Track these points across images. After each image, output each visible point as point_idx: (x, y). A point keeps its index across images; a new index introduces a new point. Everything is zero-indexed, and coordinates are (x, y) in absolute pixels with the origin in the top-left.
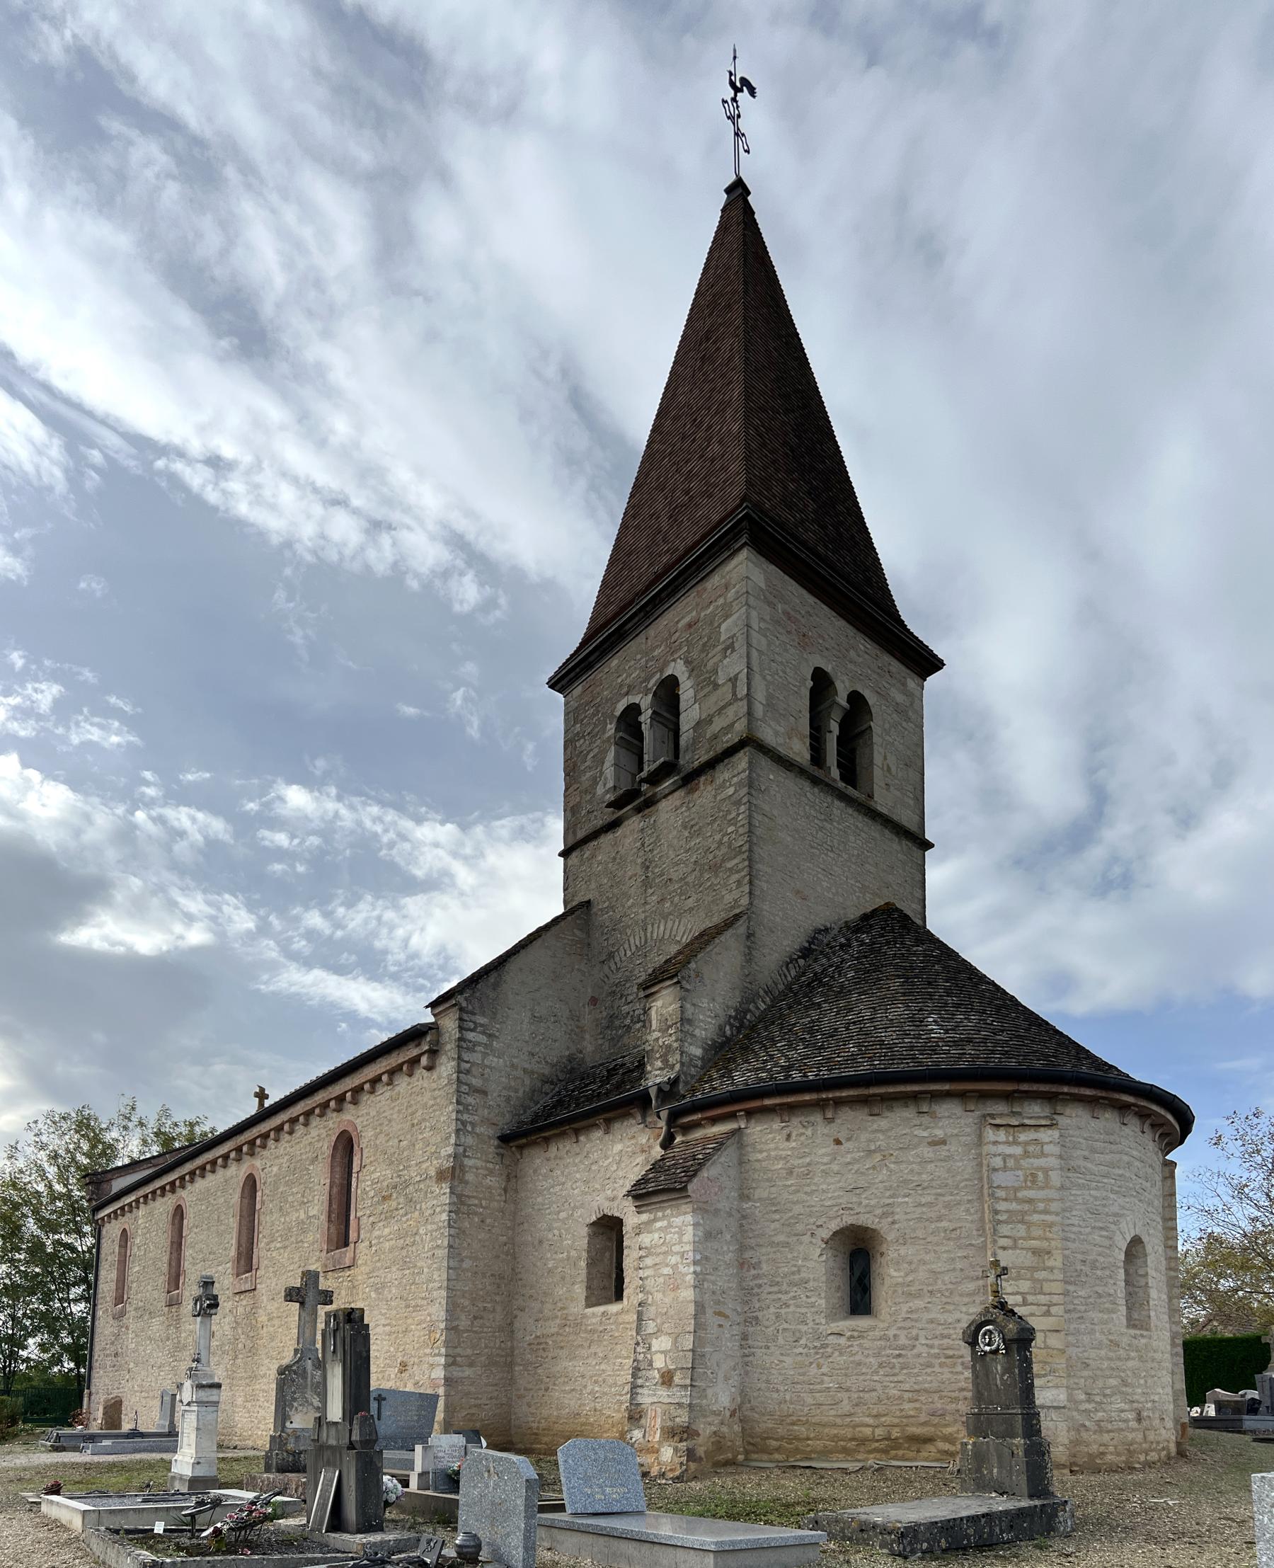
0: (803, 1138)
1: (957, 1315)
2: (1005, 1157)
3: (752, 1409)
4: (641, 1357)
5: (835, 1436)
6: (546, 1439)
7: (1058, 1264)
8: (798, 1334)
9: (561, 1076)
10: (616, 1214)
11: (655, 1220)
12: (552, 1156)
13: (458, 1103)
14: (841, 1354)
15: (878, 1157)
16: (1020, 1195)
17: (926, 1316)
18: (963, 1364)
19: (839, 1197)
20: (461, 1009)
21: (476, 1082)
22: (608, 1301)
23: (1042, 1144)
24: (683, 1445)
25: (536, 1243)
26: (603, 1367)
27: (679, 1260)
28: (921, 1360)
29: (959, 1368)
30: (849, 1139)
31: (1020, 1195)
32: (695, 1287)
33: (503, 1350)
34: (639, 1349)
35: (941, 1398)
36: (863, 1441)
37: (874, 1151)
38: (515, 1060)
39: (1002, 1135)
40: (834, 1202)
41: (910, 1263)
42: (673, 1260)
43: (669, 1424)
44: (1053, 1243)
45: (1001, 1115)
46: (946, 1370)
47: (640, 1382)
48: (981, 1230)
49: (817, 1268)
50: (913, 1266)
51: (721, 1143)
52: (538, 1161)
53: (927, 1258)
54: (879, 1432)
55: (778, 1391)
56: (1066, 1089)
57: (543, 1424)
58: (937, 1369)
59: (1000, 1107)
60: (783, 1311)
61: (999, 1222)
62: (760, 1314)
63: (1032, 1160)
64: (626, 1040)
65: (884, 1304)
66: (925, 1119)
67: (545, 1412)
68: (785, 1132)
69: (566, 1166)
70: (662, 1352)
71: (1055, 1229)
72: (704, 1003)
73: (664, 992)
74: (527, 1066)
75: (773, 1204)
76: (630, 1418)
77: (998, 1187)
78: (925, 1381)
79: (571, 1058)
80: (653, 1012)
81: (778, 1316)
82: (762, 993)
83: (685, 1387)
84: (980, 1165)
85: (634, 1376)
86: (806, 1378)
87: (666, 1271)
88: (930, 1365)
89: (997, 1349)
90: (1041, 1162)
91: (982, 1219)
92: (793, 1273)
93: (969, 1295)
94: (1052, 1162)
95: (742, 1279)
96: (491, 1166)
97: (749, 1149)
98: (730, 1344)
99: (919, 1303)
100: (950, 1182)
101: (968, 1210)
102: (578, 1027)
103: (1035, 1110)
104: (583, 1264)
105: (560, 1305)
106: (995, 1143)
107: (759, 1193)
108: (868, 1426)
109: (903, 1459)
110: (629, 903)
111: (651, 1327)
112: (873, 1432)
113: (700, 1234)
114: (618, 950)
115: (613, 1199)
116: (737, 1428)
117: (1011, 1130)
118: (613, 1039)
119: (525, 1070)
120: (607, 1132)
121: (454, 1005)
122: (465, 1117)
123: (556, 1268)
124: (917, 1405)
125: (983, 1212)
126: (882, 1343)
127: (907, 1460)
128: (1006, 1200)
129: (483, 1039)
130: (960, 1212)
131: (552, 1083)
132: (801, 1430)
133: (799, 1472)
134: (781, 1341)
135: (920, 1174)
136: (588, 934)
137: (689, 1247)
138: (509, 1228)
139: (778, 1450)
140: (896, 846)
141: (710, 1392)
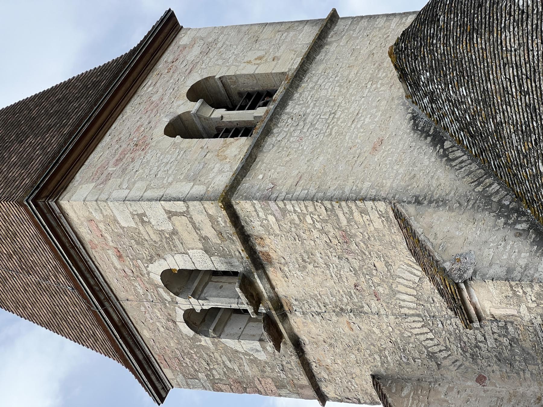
73: (476, 299)
80: (498, 312)
82: (480, 189)
110: (377, 331)
118: (525, 360)
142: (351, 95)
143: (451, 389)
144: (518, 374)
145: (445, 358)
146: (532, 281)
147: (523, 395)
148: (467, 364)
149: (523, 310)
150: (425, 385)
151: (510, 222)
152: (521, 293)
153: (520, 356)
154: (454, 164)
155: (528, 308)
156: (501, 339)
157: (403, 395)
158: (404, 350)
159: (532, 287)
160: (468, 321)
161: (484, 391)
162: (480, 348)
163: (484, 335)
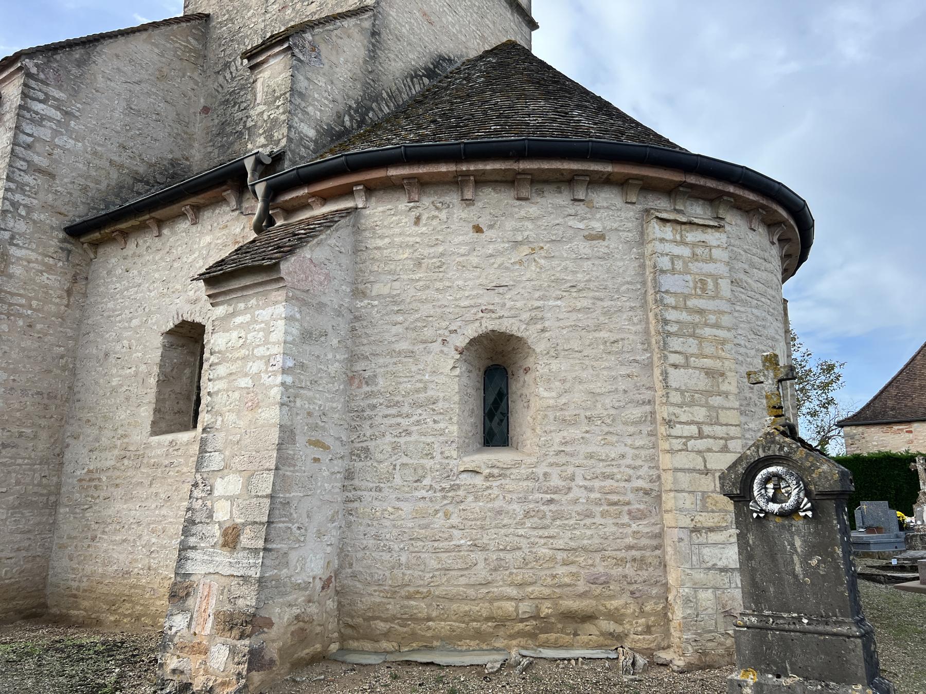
0: (435, 222)
1: (621, 449)
2: (673, 258)
3: (354, 576)
4: (197, 505)
5: (466, 614)
6: (86, 604)
7: (733, 388)
8: (420, 472)
9: (160, 178)
10: (198, 320)
11: (234, 314)
12: (130, 253)
13: (9, 179)
14: (477, 499)
15: (525, 250)
16: (690, 303)
17: (584, 449)
18: (629, 513)
19: (478, 296)
20: (29, 75)
21: (40, 160)
22: (185, 428)
23: (711, 248)
24: (244, 645)
25: (101, 356)
26: (164, 511)
27: (263, 367)
28: (579, 508)
29: (625, 519)
30: (491, 227)
31: (690, 303)
32: (282, 405)
33: (45, 487)
34: (197, 493)
35: (603, 559)
36: (502, 621)
37: (520, 243)
38: (99, 149)
39: (668, 232)
40: (472, 302)
41: (564, 381)
42: (255, 367)
43: (228, 607)
44: (727, 363)
45: (666, 211)
46: (610, 521)
47: (192, 541)
48: (646, 342)
49: (450, 386)
50: (567, 385)
51: (329, 222)
52: (113, 260)
53: (584, 375)
54: (525, 607)
55: (390, 550)
56: (731, 189)
57: (85, 584)
58: (598, 520)
59: (661, 204)
60: (402, 440)
61: (669, 334)
62: (371, 445)
63: (700, 264)
64: (236, 147)
65: (529, 433)
66: (581, 208)
67: (89, 569)
68: (414, 214)
69: (144, 265)
70: (231, 497)
71: (728, 347)
72: (321, 82)
73: (272, 62)
74: (116, 158)
75: (395, 303)
76: (173, 596)
77: (667, 292)
78: (583, 537)
79: (174, 163)
80: (259, 85)
81: (395, 447)
82: (385, 95)
83: (255, 551)
84: (643, 266)
85: (186, 532)
86: (428, 532)
87: (244, 382)
88: (589, 515)
89: (797, 509)
90: (709, 268)
91: (647, 332)
92: (417, 391)
93: (634, 423)
94: (722, 269)
95: (351, 398)
96: (51, 261)
97: (367, 234)
98: (327, 484)
99: (574, 433)
100: (610, 284)
101: (630, 319)
102: (186, 133)
103: (697, 211)
104: (153, 381)
105: (120, 432)
106: (662, 240)
107: (379, 289)
108: (510, 599)
109: (556, 646)
110: (249, 14)
111: (215, 461)
112: (517, 608)
113: (295, 332)
114: (234, 60)
115: (195, 302)
116: (331, 604)
117: (678, 227)
118: (223, 146)
119: (111, 162)
120: (194, 223)
121: (20, 69)
122: (18, 197)
123: (122, 385)
124: (573, 569)
125: (648, 323)
126: (530, 484)
127: (561, 647)
128: (675, 308)
129: (58, 115)
130: (622, 320)
131: (147, 183)
132: (420, 607)
133: (415, 671)
134: (398, 481)
135: (574, 273)
136: (205, 46)
137: (277, 349)
138: (70, 338)
139: (386, 635)
140: (509, 14)
141: (293, 556)
142: (471, 14)
143: (196, 83)
144: (211, 141)
145: (225, 77)
146: (290, 112)
147: (191, 146)
148: (220, 97)
149: (259, 109)
150: (200, 61)
151: (352, 112)
152: (277, 104)
153: (226, 141)
154: (409, 80)
155: (263, 113)
156: (242, 123)
157: (189, 38)
158: (232, 41)
159: (284, 113)
160: (250, 55)
161: (195, 113)
162: (234, 106)
163: (245, 109)
